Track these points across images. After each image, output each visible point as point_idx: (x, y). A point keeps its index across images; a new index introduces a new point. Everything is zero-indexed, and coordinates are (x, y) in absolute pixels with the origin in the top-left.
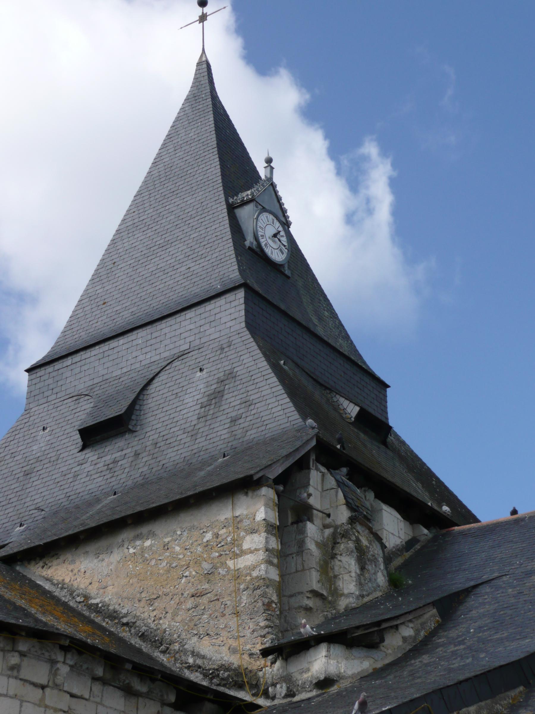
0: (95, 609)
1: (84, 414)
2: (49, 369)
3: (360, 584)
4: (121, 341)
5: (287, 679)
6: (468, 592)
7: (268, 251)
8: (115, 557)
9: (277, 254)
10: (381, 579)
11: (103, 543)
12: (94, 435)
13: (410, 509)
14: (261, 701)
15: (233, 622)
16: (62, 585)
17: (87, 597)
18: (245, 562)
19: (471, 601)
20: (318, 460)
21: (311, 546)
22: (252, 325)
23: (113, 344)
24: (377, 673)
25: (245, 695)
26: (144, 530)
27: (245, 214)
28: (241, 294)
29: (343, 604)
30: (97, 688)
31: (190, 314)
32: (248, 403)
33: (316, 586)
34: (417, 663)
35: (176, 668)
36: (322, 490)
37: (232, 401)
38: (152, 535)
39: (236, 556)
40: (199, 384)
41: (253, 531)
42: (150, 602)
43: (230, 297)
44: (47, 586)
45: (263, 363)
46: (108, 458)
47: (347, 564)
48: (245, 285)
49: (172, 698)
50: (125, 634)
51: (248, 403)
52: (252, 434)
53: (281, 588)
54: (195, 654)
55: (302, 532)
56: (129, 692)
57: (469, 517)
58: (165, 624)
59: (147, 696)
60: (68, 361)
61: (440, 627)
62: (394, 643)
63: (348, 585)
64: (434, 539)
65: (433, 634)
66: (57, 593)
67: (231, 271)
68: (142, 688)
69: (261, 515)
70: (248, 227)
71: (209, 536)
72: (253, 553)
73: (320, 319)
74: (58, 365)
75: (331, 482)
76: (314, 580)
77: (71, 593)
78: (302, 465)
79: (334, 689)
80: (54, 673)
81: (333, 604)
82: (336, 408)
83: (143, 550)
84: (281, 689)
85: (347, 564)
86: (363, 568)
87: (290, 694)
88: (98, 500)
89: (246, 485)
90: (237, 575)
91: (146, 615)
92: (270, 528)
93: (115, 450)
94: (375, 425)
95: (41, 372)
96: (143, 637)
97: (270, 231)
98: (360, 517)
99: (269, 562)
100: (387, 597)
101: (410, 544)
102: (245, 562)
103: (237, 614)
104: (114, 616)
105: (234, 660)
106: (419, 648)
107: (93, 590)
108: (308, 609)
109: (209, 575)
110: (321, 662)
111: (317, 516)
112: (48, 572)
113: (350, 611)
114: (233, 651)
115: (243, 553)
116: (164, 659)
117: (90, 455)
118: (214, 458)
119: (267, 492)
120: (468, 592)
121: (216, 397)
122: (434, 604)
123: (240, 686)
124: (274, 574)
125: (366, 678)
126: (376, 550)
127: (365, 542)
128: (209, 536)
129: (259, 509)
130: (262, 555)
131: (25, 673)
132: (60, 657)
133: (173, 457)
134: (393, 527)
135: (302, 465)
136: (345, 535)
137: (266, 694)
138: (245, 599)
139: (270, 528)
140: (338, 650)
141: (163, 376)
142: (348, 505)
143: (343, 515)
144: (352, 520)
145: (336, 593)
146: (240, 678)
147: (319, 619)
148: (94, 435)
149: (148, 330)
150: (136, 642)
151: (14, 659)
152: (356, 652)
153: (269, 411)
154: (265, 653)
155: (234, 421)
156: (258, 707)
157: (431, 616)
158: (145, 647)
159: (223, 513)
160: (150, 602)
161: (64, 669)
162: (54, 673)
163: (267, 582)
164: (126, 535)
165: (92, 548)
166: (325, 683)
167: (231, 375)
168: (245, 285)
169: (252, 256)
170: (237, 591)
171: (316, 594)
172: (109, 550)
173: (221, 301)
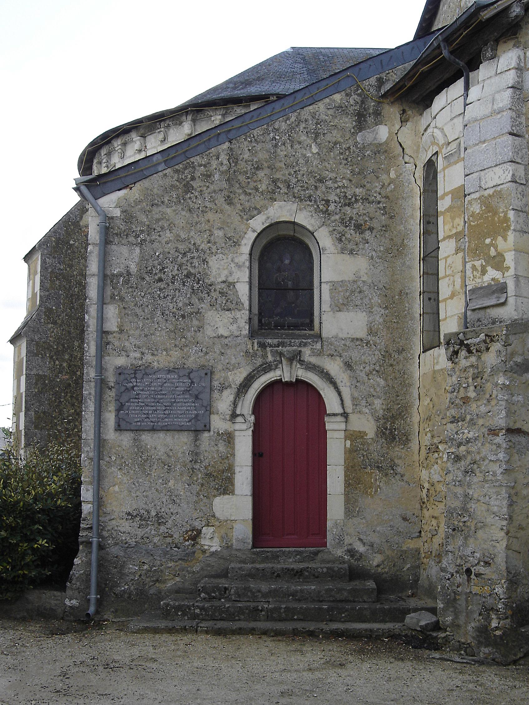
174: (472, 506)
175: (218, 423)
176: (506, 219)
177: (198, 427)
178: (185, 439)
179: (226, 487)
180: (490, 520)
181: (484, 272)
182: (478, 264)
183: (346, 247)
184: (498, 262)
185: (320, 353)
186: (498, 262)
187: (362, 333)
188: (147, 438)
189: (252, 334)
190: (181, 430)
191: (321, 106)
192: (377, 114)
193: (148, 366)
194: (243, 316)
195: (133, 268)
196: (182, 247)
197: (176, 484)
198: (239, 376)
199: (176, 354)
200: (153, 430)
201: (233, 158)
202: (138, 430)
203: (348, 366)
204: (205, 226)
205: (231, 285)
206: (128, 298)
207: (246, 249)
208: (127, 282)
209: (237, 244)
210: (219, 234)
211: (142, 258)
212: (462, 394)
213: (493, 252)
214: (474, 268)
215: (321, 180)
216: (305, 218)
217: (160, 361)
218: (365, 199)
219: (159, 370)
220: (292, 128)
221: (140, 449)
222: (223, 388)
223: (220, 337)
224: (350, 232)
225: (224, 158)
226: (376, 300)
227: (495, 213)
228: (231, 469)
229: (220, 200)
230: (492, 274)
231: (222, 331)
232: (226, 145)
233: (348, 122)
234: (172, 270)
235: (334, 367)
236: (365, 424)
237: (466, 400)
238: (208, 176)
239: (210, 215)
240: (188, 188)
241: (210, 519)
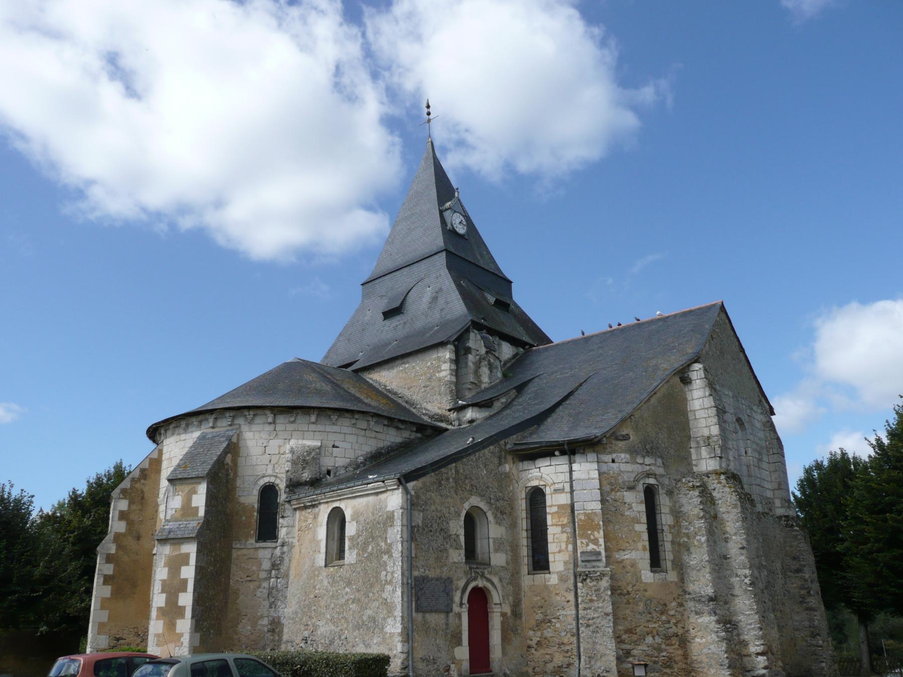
0: (389, 391)
1: (384, 305)
2: (370, 284)
3: (490, 378)
4: (398, 273)
5: (459, 419)
6: (530, 381)
7: (457, 230)
8: (395, 370)
9: (461, 230)
10: (499, 375)
11: (390, 365)
12: (388, 314)
13: (514, 341)
14: (450, 427)
15: (439, 398)
16: (376, 381)
17: (386, 386)
18: (443, 374)
19: (530, 385)
20: (474, 328)
21: (470, 364)
22: (450, 267)
23: (394, 274)
24: (491, 417)
25: (443, 425)
26: (405, 360)
27: (447, 214)
28: (444, 253)
29: (483, 386)
30: (385, 428)
31: (424, 261)
32: (447, 303)
33: (472, 380)
34: (504, 413)
35: (419, 414)
36: (475, 341)
37: (441, 301)
38: (408, 362)
39: (439, 372)
40: (429, 293)
41: (445, 362)
42: (409, 389)
43: (440, 254)
44: (371, 382)
45: (453, 285)
46: (394, 325)
47: (485, 371)
48: (446, 250)
49: (415, 429)
50: (400, 401)
51: (447, 303)
52: (449, 317)
53: (457, 384)
54: (426, 409)
55: (467, 358)
56: (398, 428)
57: (544, 339)
58: (414, 397)
59: (405, 429)
60: (377, 281)
61: (516, 397)
62: (497, 405)
63: (485, 379)
64: (525, 354)
65: (513, 400)
66: (375, 384)
67: (440, 242)
68: (403, 427)
69: (448, 356)
70: (448, 221)
71: (429, 364)
72: (445, 371)
73: (482, 256)
74: (373, 283)
75: (479, 337)
76: (471, 378)
77: (380, 384)
78: (467, 331)
79: (474, 424)
80: (369, 425)
81: (480, 386)
82: (486, 299)
83: (405, 368)
84: (457, 423)
85: (485, 371)
86: (491, 372)
87: (460, 425)
88: (390, 344)
89: (442, 344)
90: (440, 379)
91: (407, 394)
92: (451, 361)
93: (396, 321)
94: (505, 305)
95: (367, 285)
96: (407, 402)
97: (458, 221)
98: (490, 350)
99: (451, 374)
100: (501, 382)
101: (514, 356)
102: (443, 374)
103: (440, 394)
104: (395, 394)
105: (440, 412)
106: (507, 406)
107: (387, 383)
108: (470, 389)
109: (430, 379)
110: (470, 414)
111: (474, 352)
112: (371, 376)
113: (487, 389)
114: (439, 408)
115: (442, 371)
116: (414, 411)
117: (387, 322)
118: (433, 327)
119: (450, 347)
120: (530, 381)
121: (435, 299)
122: (514, 388)
123: (442, 421)
124: (454, 379)
125: (487, 419)
126: (497, 363)
127: (492, 361)
128: (429, 364)
129: (447, 354)
130: (448, 372)
131: (358, 426)
132: (370, 419)
133: (419, 325)
134: (507, 351)
135: (467, 331)
136: (484, 359)
137: (451, 424)
138: (443, 389)
139: (451, 361)
140: (476, 409)
141: (414, 289)
142: (485, 346)
143: (483, 351)
144: (487, 353)
145: (481, 382)
146: (442, 418)
147: (474, 393)
148: (388, 314)
149: (408, 268)
150: (404, 404)
151: (354, 421)
152: (483, 409)
153: (455, 307)
154: (450, 410)
155: (442, 310)
156: (447, 430)
157: (513, 393)
158: (407, 406)
159: (434, 355)
160: (409, 389)
161: (372, 423)
162: (369, 425)
163: (451, 382)
164: (399, 362)
165: (386, 367)
166: (471, 421)
167: (441, 290)
168: (446, 250)
169: (450, 233)
170: (440, 386)
171: (472, 383)
172: (393, 368)
173: (436, 257)
174: (598, 647)
175: (456, 609)
176: (599, 524)
177: (448, 611)
178: (443, 616)
179: (459, 643)
180: (608, 652)
181: (587, 545)
182: (584, 541)
183: (499, 523)
184: (595, 542)
185: (490, 573)
186: (595, 542)
187: (504, 564)
188: (427, 615)
189: (466, 563)
190: (441, 612)
191: (486, 451)
192: (505, 458)
193: (427, 577)
194: (463, 552)
195: (420, 525)
196: (439, 515)
197: (440, 641)
198: (462, 584)
199: (438, 571)
200: (431, 611)
201: (457, 472)
202: (426, 612)
203: (501, 580)
204: (447, 505)
205: (458, 536)
206: (419, 539)
207: (463, 518)
208: (418, 530)
209: (459, 515)
210: (452, 509)
211: (424, 519)
212: (589, 597)
213: (592, 537)
214: (582, 543)
215: (488, 487)
216: (483, 505)
217: (432, 574)
218: (503, 499)
219: (432, 579)
220: (477, 460)
221: (425, 622)
222: (457, 589)
223: (454, 563)
224: (499, 515)
225: (453, 471)
226: (509, 548)
227: (593, 521)
228: (460, 633)
229: (453, 492)
230: (591, 547)
231: (456, 560)
232: (454, 465)
233: (496, 461)
234: (435, 526)
235: (496, 580)
236: (507, 609)
237: (591, 601)
238: (448, 479)
239: (449, 500)
240: (440, 484)
241: (453, 660)
